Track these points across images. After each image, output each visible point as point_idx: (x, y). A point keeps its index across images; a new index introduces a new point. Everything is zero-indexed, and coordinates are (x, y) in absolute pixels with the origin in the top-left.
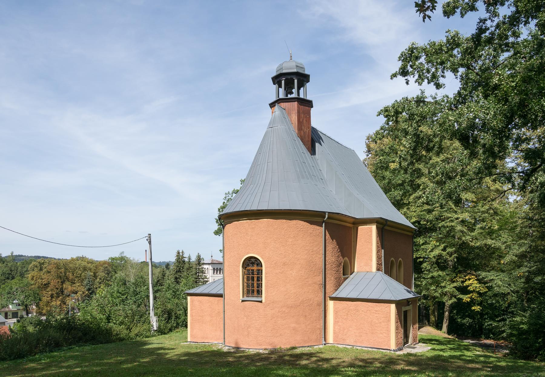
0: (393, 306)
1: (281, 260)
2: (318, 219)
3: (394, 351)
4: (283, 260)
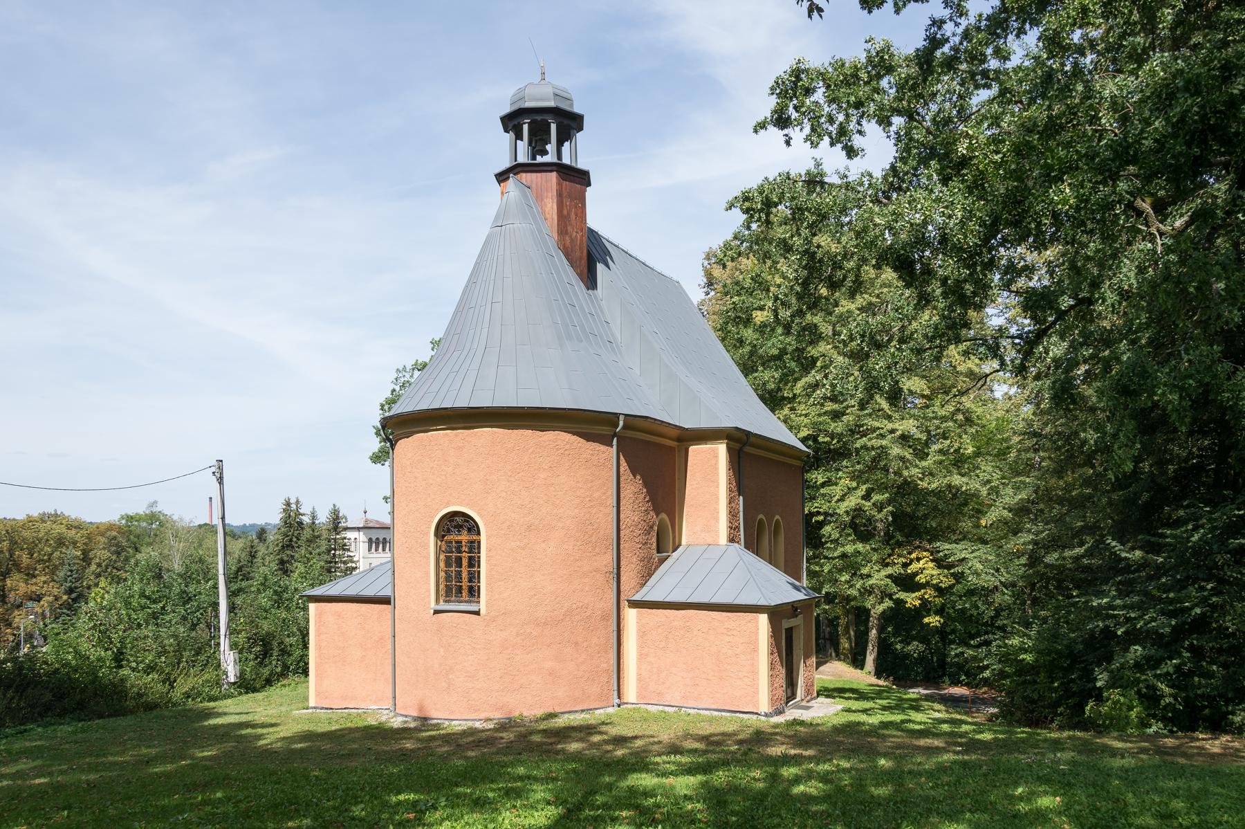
0: (763, 619)
1: (522, 520)
2: (582, 428)
3: (766, 715)
4: (527, 519)
